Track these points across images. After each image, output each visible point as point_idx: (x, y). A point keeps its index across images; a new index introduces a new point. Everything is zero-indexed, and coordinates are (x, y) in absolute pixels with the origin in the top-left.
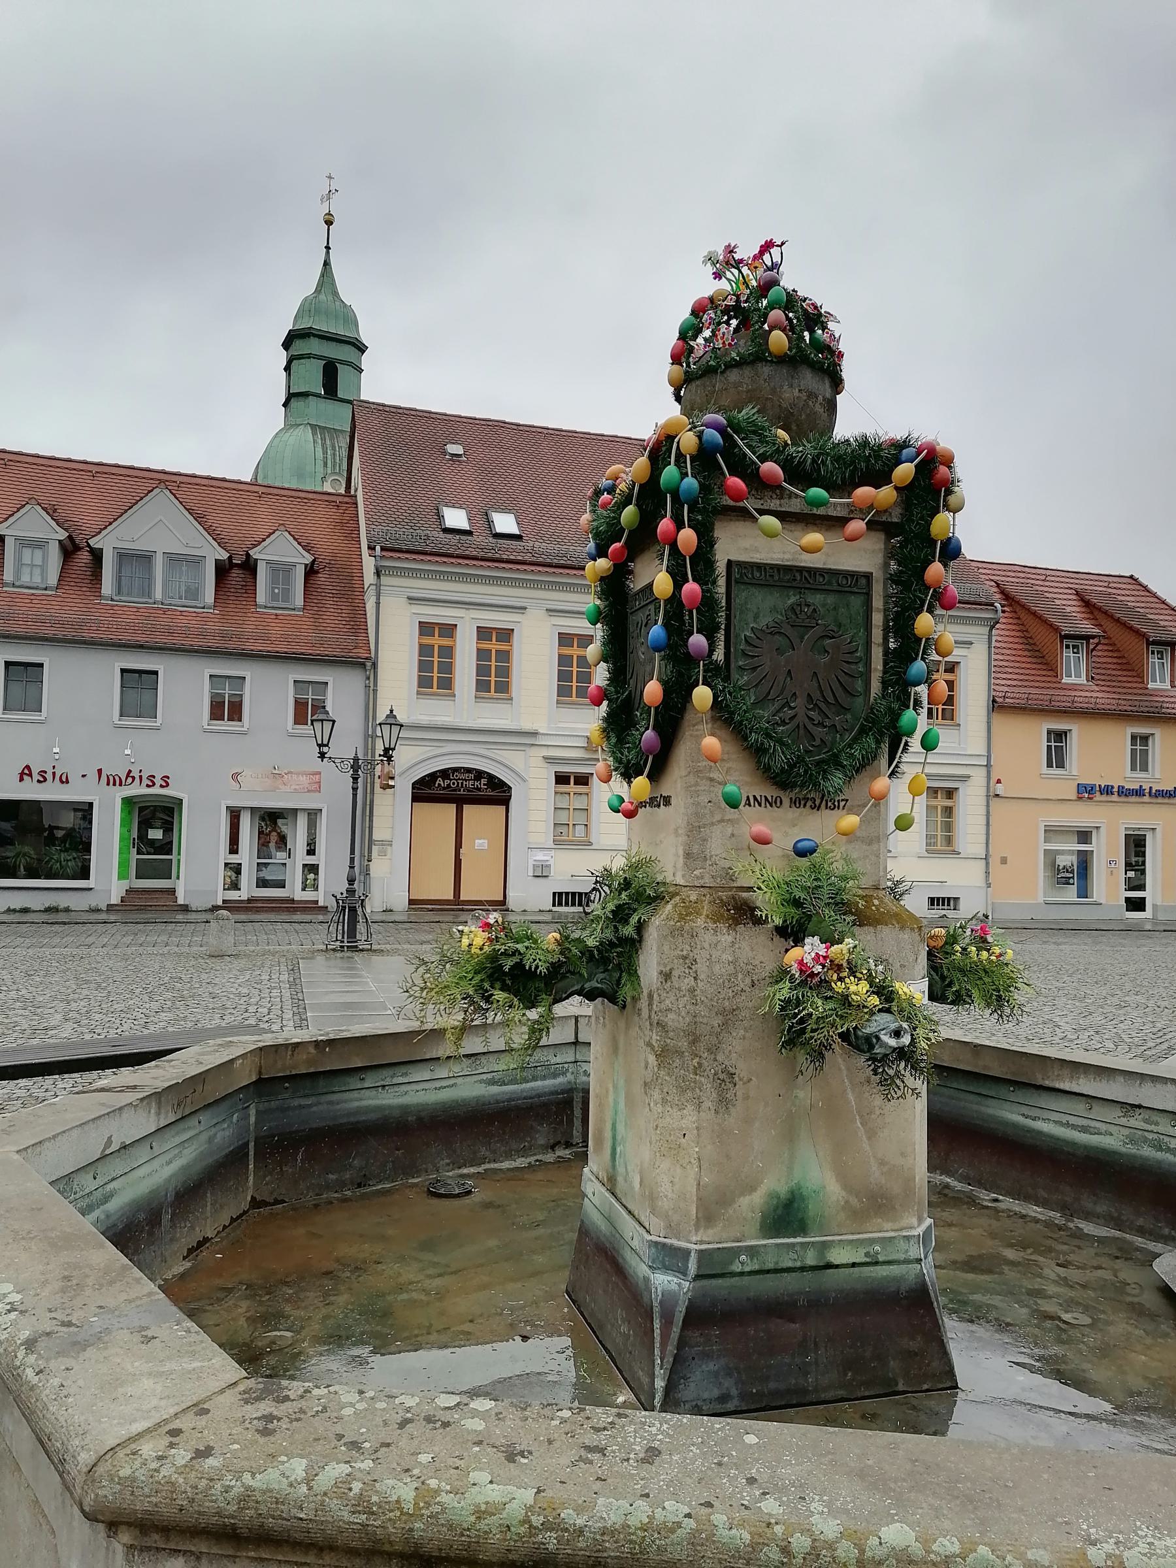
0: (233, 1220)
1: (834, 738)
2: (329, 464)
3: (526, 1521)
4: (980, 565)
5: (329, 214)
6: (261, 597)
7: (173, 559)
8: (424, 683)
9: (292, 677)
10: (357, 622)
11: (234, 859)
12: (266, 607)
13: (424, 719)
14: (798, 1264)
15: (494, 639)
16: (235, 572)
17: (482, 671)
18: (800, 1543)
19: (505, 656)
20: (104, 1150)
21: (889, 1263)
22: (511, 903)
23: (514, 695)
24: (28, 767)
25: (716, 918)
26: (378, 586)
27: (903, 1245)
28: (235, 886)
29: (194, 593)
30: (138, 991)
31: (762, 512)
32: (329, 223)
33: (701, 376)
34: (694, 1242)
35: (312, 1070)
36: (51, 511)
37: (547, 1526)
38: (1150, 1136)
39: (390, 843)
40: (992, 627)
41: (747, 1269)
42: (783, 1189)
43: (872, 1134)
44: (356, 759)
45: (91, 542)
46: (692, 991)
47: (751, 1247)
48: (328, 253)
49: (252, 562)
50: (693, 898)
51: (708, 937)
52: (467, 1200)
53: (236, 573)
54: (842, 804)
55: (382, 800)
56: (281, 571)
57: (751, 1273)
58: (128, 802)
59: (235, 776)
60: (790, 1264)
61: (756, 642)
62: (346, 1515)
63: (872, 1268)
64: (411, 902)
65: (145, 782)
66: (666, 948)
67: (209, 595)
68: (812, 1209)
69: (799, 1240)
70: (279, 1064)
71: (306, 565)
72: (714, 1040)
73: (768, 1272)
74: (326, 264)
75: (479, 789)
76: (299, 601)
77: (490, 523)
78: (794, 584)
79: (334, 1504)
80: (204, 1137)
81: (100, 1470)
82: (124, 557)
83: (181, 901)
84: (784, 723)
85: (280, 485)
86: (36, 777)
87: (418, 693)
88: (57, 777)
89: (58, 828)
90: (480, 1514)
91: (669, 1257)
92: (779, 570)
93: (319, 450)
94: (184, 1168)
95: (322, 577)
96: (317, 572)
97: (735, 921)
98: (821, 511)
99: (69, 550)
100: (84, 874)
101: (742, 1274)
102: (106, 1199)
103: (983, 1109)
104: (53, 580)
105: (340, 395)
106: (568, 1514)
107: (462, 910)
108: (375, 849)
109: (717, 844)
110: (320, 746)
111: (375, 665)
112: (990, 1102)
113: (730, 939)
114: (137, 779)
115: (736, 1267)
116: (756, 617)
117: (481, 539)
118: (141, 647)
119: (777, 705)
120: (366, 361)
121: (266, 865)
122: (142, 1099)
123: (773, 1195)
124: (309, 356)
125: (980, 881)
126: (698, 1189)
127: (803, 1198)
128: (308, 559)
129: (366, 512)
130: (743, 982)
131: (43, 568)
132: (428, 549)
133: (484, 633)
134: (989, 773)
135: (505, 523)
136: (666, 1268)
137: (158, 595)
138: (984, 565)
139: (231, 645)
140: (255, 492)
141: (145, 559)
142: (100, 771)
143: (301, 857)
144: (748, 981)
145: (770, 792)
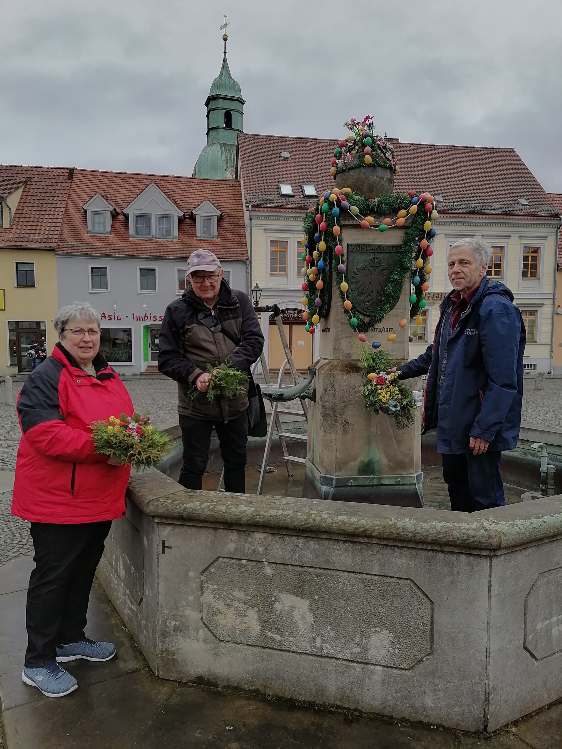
2: (229, 163)
3: (252, 514)
4: (554, 196)
5: (225, 35)
6: (199, 232)
7: (160, 218)
10: (242, 243)
16: (187, 221)
18: (318, 519)
24: (104, 313)
25: (342, 370)
26: (251, 224)
29: (169, 232)
30: (154, 407)
32: (225, 40)
33: (341, 172)
34: (334, 476)
36: (106, 197)
37: (257, 515)
38: (531, 452)
40: (559, 228)
41: (353, 485)
42: (366, 460)
43: (399, 443)
46: (334, 395)
48: (225, 55)
49: (194, 216)
50: (335, 364)
52: (272, 474)
53: (187, 221)
56: (207, 219)
57: (354, 486)
58: (146, 327)
61: (358, 273)
62: (209, 513)
65: (153, 319)
66: (325, 381)
67: (176, 233)
72: (341, 411)
73: (361, 486)
74: (225, 61)
76: (216, 233)
77: (303, 191)
78: (372, 251)
79: (206, 510)
81: (150, 503)
82: (138, 217)
84: (368, 301)
86: (107, 318)
87: (270, 274)
89: (117, 339)
90: (241, 513)
91: (327, 481)
93: (224, 156)
95: (225, 221)
96: (223, 219)
97: (349, 372)
99: (115, 215)
100: (129, 359)
101: (351, 486)
104: (109, 230)
106: (262, 513)
109: (344, 345)
111: (250, 262)
113: (347, 377)
114: (149, 318)
116: (358, 263)
117: (299, 199)
118: (148, 258)
119: (366, 295)
120: (245, 108)
123: (362, 462)
124: (217, 109)
125: (547, 355)
127: (373, 463)
128: (219, 213)
129: (245, 189)
130: (351, 392)
131: (104, 224)
132: (273, 206)
134: (554, 302)
135: (310, 190)
136: (326, 484)
137: (154, 233)
138: (557, 196)
140: (195, 182)
141: (147, 218)
142: (133, 314)
144: (353, 391)
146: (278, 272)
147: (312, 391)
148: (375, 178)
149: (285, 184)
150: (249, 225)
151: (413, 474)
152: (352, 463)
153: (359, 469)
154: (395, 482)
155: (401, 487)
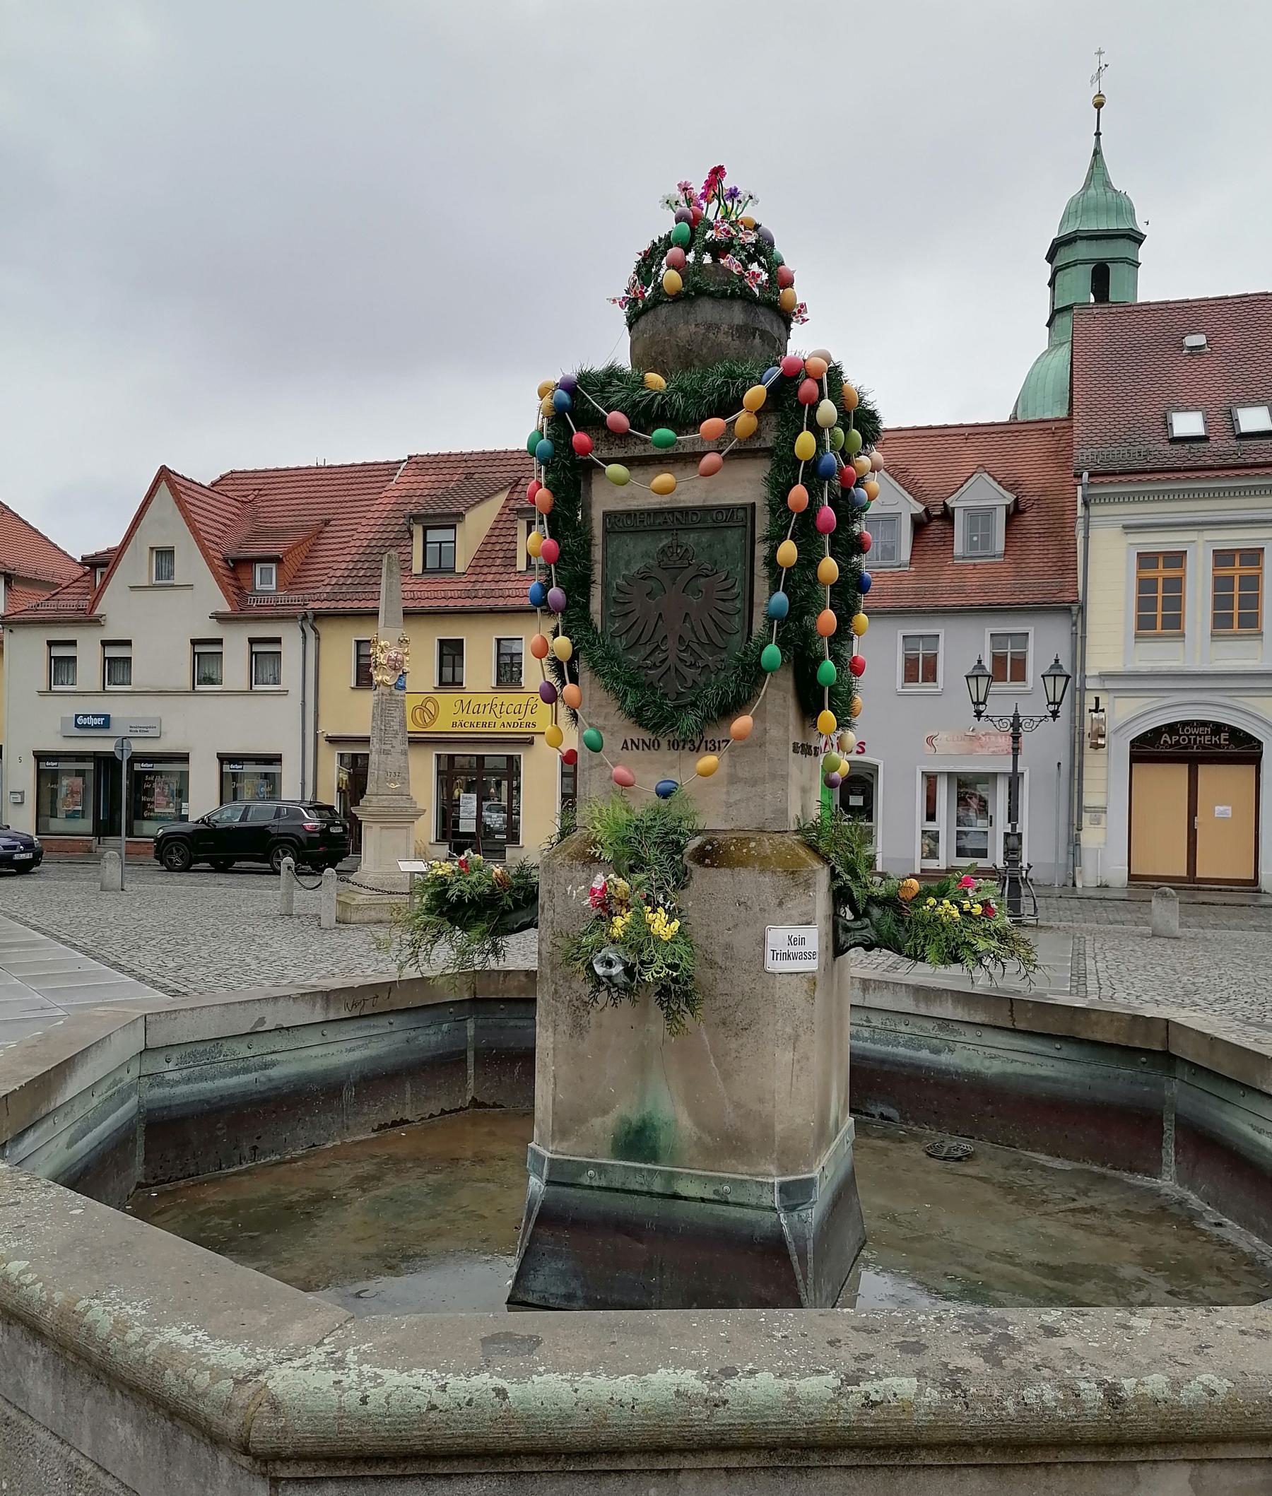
0: (443, 1112)
1: (709, 678)
5: (1100, 95)
6: (958, 548)
8: (1144, 624)
9: (989, 631)
11: (931, 826)
12: (964, 558)
13: (1144, 666)
14: (645, 1188)
15: (1161, 565)
17: (1221, 602)
19: (1253, 583)
20: (255, 1026)
21: (741, 1205)
22: (1264, 883)
23: (1264, 630)
26: (1087, 518)
27: (755, 1190)
28: (933, 854)
31: (609, 461)
32: (1099, 105)
35: (523, 996)
39: (1104, 810)
41: (594, 1184)
42: (635, 1118)
43: (727, 1077)
44: (1016, 717)
45: (947, 502)
47: (600, 1164)
48: (1098, 140)
51: (564, 873)
54: (723, 745)
55: (1093, 761)
56: (980, 516)
57: (600, 1188)
59: (930, 740)
60: (637, 1187)
61: (628, 589)
63: (724, 1208)
64: (1132, 877)
67: (905, 553)
68: (663, 1139)
69: (650, 1166)
70: (492, 988)
71: (1008, 506)
73: (617, 1190)
74: (1097, 152)
75: (1218, 746)
76: (999, 544)
80: (401, 1036)
83: (879, 869)
84: (654, 666)
85: (1037, 418)
87: (1212, 635)
92: (649, 514)
94: (373, 1059)
96: (1024, 512)
98: (671, 451)
101: (591, 1188)
102: (266, 1066)
103: (1216, 1112)
105: (1112, 298)
107: (1198, 889)
108: (1086, 817)
110: (977, 703)
111: (1082, 609)
112: (1227, 1107)
113: (584, 875)
115: (585, 1180)
116: (627, 564)
117: (1222, 445)
119: (649, 649)
120: (1143, 253)
121: (966, 833)
122: (302, 994)
123: (624, 1120)
126: (554, 1104)
127: (654, 1128)
128: (1009, 498)
132: (1149, 466)
133: (1222, 557)
135: (1253, 419)
139: (927, 602)
143: (1002, 825)
145: (647, 736)
146: (1159, 630)
148: (692, 328)
151: (770, 1175)
152: (597, 1122)
153: (615, 1140)
154: (716, 1192)
155: (736, 1213)
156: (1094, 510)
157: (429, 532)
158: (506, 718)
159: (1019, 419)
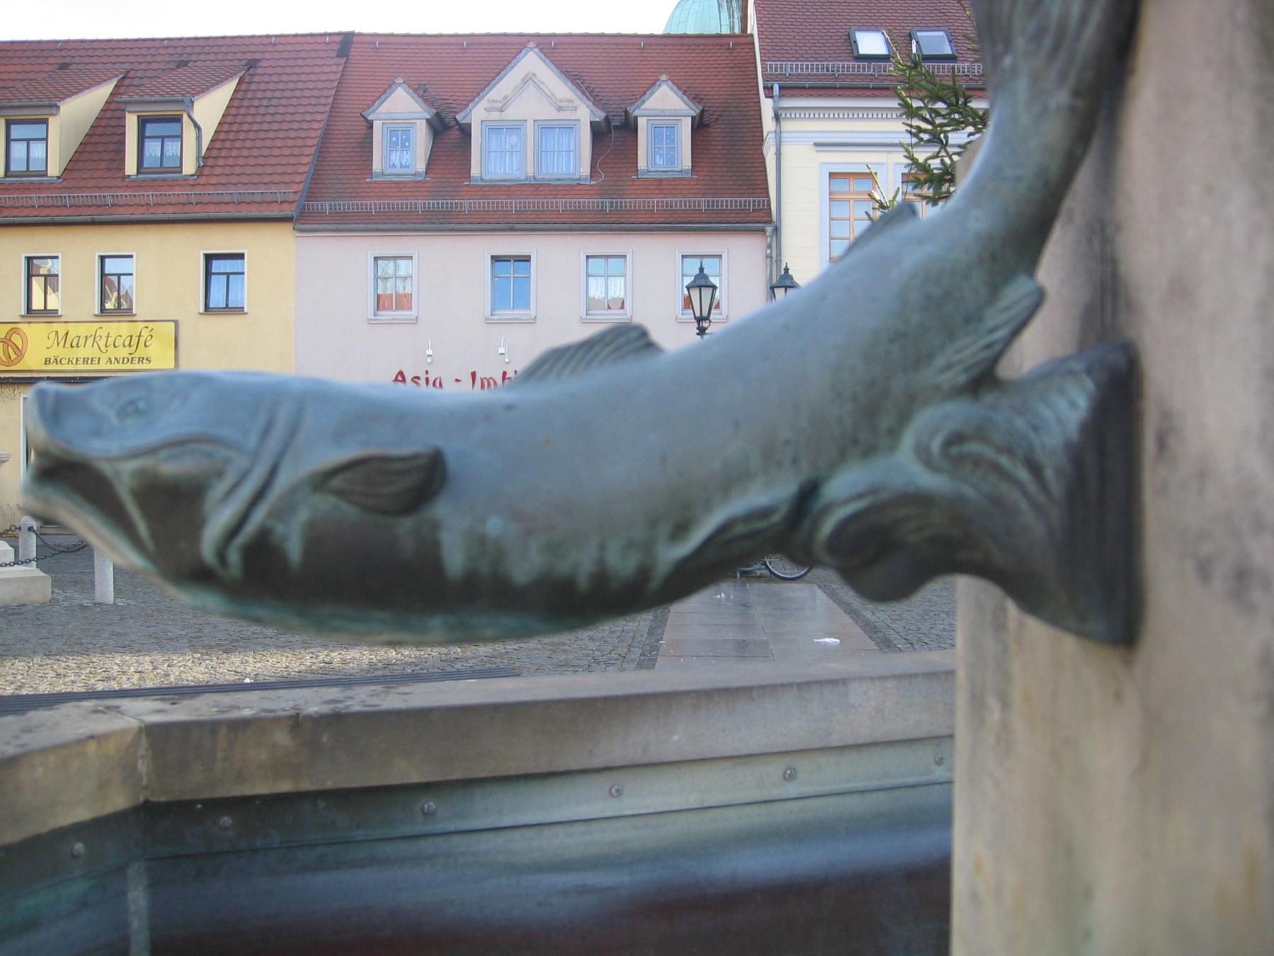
24: (401, 373)
35: (285, 786)
49: (632, 120)
53: (615, 136)
56: (665, 128)
82: (494, 129)
88: (431, 382)
93: (725, 14)
96: (707, 126)
111: (777, 230)
142: (474, 375)
147: (1070, 408)
149: (868, 30)
150: (772, 136)
156: (787, 126)
157: (13, 127)
158: (112, 352)
159: (392, 263)
